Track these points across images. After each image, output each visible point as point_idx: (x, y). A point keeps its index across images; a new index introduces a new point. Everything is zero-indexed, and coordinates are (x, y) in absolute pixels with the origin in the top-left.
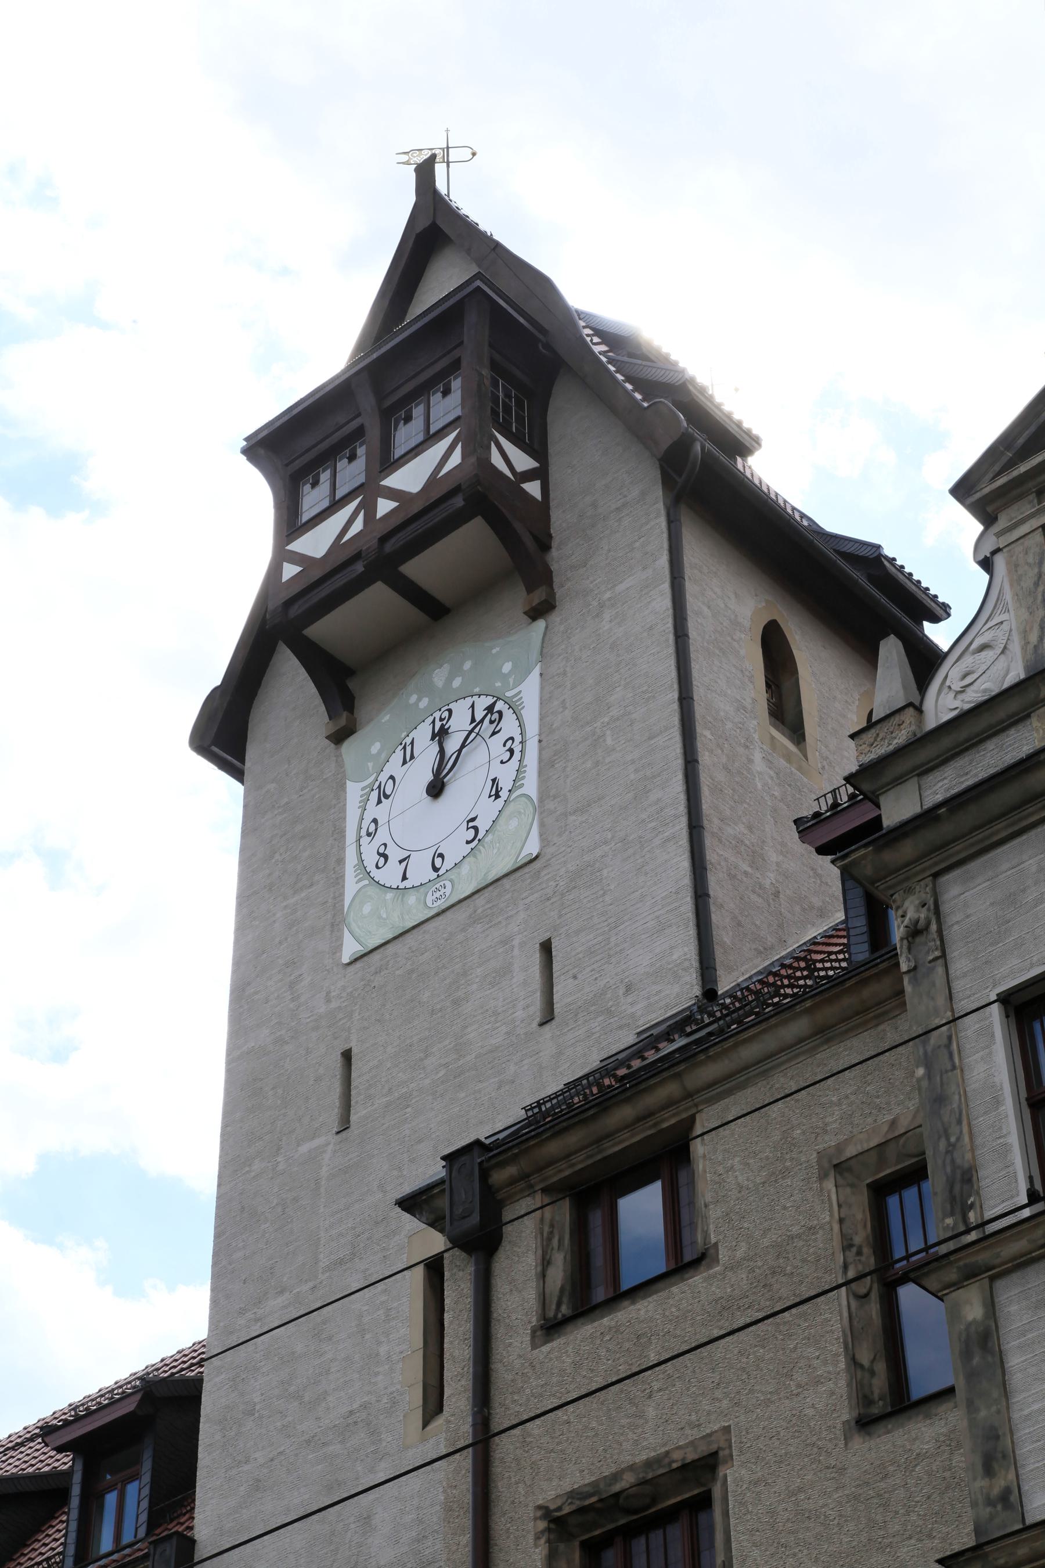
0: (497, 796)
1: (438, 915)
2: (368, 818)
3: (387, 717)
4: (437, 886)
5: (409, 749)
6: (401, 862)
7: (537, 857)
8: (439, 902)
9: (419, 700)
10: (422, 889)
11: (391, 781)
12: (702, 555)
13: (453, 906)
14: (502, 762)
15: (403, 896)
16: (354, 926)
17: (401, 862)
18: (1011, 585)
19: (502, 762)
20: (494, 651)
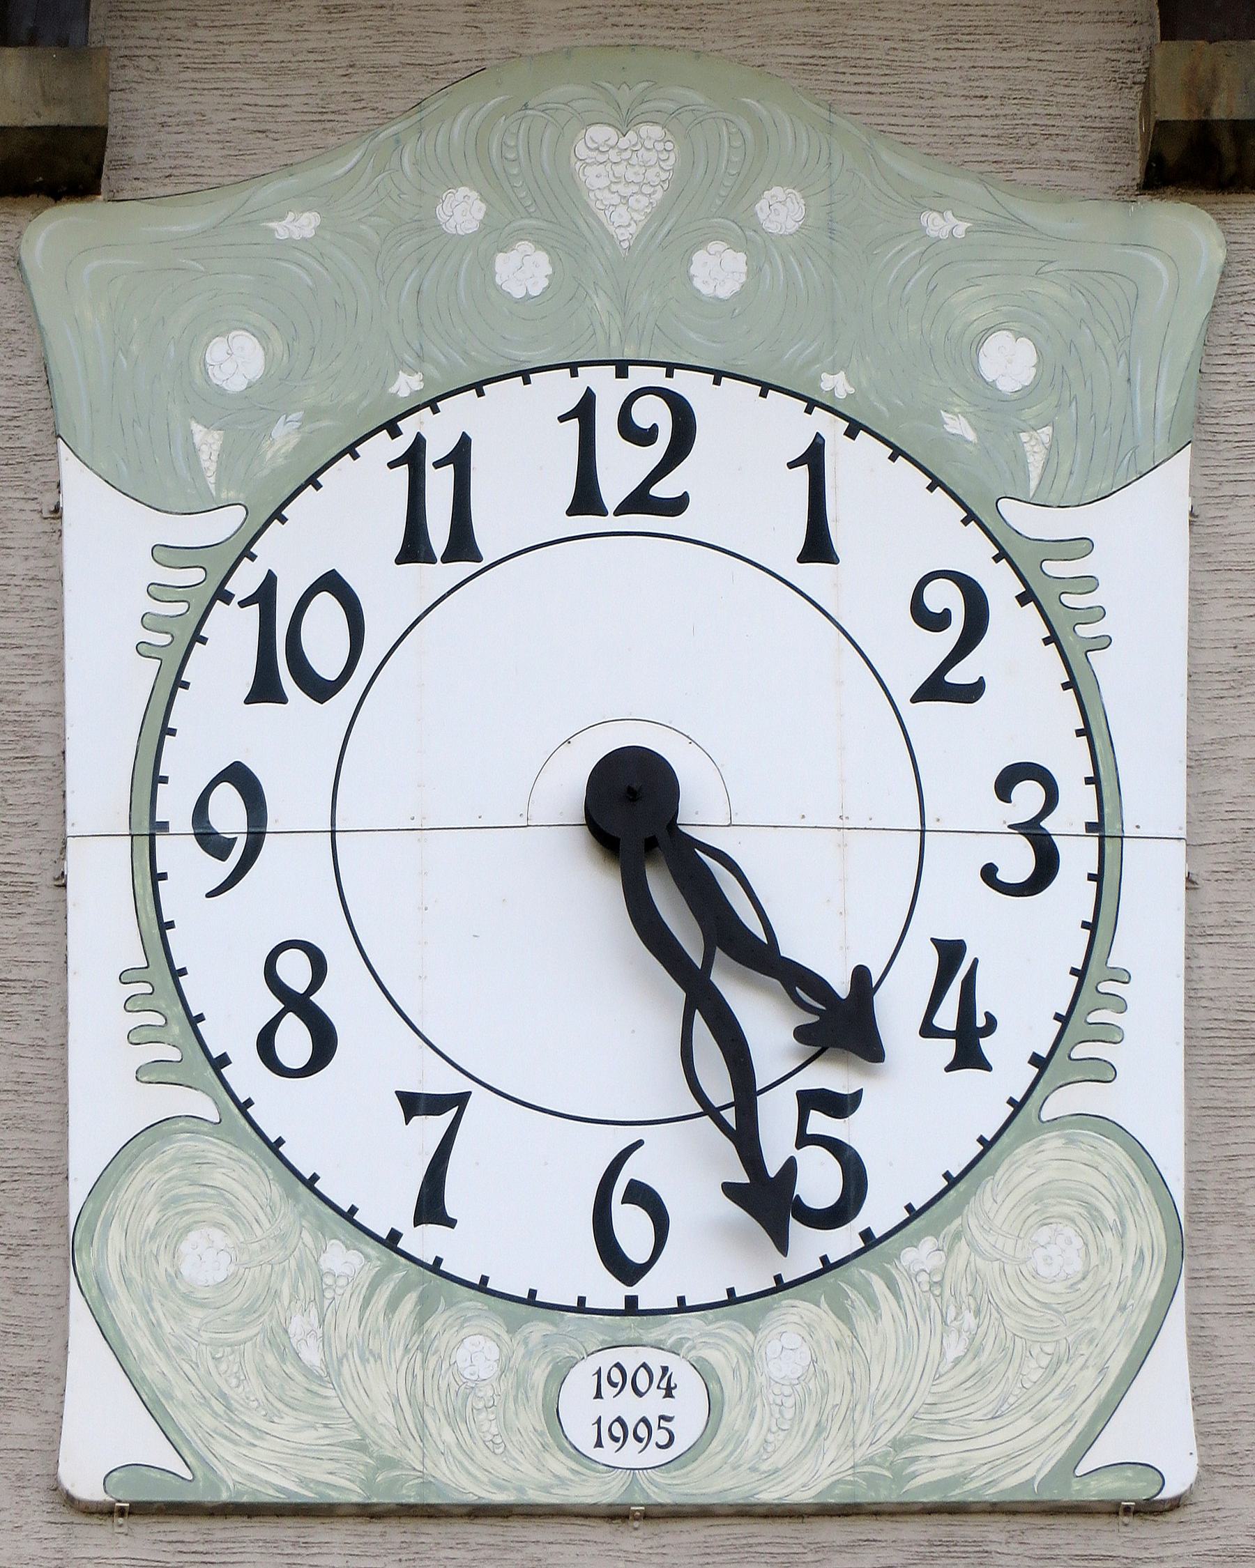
0: (969, 1054)
1: (617, 1515)
2: (188, 767)
3: (300, 225)
4: (630, 1359)
5: (439, 485)
6: (971, 693)
7: (1176, 1504)
8: (631, 1454)
9: (497, 236)
10: (539, 1328)
11: (326, 603)
12: (700, 1024)
13: (703, 1513)
14: (989, 873)
15: (424, 1312)
16: (124, 1308)
17: (971, 693)
18: (745, 1361)
19: (989, 873)
20: (938, 224)
